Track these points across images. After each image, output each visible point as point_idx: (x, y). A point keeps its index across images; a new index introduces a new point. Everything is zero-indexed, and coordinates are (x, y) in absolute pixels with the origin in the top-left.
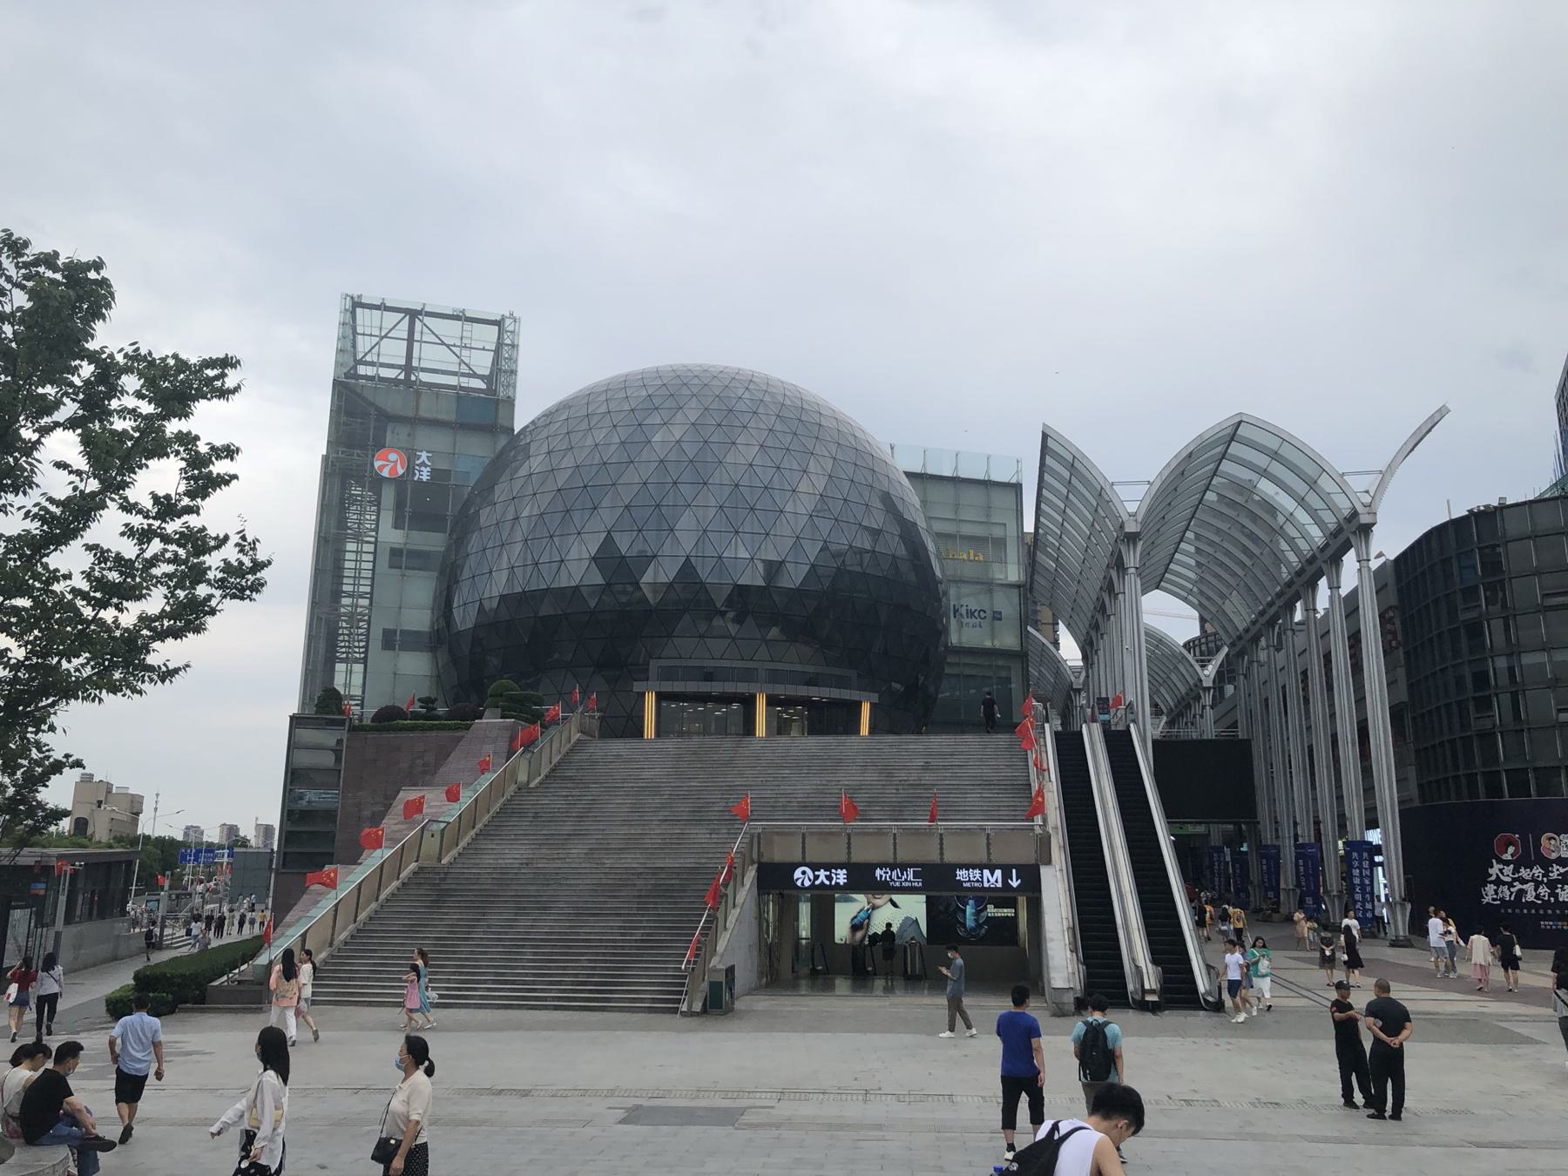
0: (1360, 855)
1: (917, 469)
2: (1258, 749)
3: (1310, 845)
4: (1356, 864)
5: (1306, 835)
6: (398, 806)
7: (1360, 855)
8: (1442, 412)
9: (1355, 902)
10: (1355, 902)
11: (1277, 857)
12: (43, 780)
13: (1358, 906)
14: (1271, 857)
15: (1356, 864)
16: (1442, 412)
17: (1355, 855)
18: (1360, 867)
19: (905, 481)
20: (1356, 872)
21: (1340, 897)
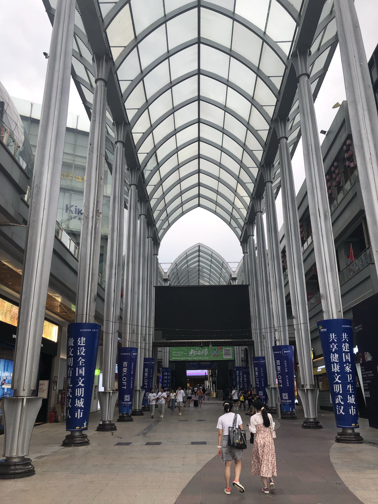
0: (339, 337)
1: (27, 114)
2: (4, 426)
3: (286, 347)
4: (334, 347)
5: (282, 339)
6: (167, 284)
7: (339, 337)
8: (193, 443)
9: (335, 395)
10: (335, 395)
11: (264, 366)
12: (160, 363)
13: (339, 399)
14: (260, 364)
15: (334, 347)
16: (193, 443)
17: (333, 336)
18: (340, 351)
19: (20, 123)
20: (335, 358)
21: (312, 391)
